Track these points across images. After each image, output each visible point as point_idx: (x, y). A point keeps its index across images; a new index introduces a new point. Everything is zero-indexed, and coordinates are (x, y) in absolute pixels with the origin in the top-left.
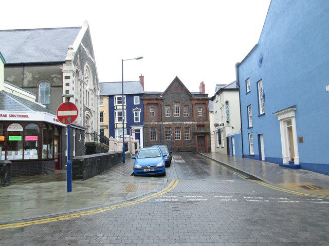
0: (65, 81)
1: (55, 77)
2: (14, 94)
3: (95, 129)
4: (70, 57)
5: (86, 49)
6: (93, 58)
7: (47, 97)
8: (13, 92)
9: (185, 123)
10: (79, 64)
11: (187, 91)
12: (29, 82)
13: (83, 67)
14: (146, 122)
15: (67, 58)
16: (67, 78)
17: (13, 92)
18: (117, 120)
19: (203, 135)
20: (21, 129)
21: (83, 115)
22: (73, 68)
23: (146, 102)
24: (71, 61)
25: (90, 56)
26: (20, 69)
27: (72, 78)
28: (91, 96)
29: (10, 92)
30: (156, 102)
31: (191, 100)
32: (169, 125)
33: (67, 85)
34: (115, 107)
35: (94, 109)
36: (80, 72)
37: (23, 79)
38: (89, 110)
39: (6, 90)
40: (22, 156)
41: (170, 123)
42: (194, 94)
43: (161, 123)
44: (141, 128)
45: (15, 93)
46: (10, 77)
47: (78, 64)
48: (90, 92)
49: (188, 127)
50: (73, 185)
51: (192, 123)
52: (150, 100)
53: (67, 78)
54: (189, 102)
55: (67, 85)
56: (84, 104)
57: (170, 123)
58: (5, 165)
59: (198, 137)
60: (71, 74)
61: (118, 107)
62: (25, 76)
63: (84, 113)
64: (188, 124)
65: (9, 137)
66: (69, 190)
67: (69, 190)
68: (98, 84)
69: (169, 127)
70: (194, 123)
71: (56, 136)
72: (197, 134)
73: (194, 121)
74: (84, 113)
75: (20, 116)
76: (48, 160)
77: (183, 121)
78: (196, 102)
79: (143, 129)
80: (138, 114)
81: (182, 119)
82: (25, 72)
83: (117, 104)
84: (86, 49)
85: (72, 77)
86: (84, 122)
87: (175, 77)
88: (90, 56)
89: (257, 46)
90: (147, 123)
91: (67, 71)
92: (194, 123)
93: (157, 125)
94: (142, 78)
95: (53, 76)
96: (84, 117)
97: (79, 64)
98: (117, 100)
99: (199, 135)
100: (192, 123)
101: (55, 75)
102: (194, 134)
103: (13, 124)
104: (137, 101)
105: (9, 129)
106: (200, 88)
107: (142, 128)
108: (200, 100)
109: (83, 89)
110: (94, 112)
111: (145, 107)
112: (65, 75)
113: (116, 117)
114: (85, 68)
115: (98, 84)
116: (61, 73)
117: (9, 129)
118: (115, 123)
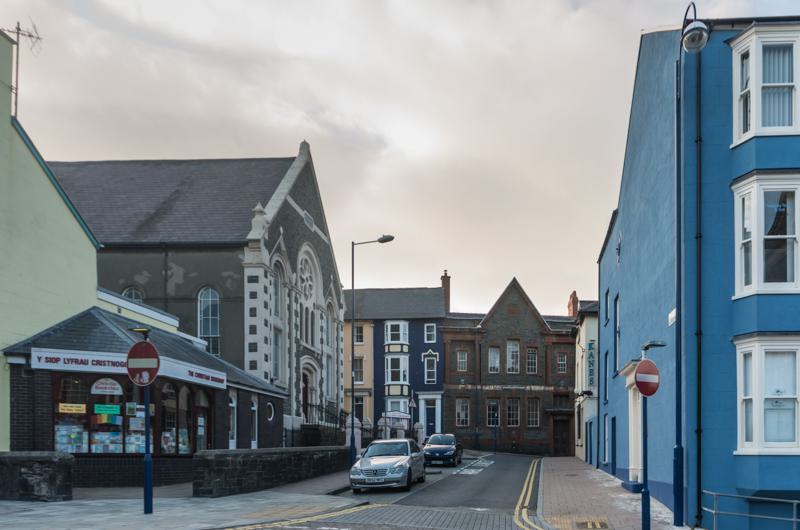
0: (249, 288)
1: (230, 277)
2: (122, 314)
3: (330, 396)
4: (257, 232)
5: (302, 213)
6: (326, 233)
7: (214, 321)
8: (119, 311)
9: (528, 388)
10: (283, 248)
11: (534, 312)
12: (178, 286)
13: (296, 254)
14: (450, 383)
15: (251, 236)
16: (254, 279)
17: (119, 311)
18: (390, 378)
19: (565, 418)
20: (118, 391)
21: (294, 365)
22: (265, 256)
23: (448, 338)
24: (258, 241)
25: (315, 228)
26: (158, 257)
27: (263, 281)
28: (318, 323)
29: (114, 310)
30: (469, 337)
31: (543, 335)
32: (495, 391)
33: (253, 295)
34: (387, 348)
35: (326, 349)
36: (287, 266)
37: (166, 281)
38: (311, 353)
39: (104, 306)
40: (121, 446)
41: (498, 387)
42: (551, 323)
43: (479, 387)
44: (437, 397)
45: (124, 313)
46: (141, 274)
47: (279, 250)
48: (317, 313)
49: (535, 397)
50: (155, 501)
51: (542, 388)
52: (474, 333)
53: (254, 279)
54: (539, 340)
55: (253, 295)
56: (296, 339)
57: (498, 387)
58: (56, 460)
59: (555, 421)
60: (259, 272)
61: (392, 349)
62: (169, 273)
63: (298, 363)
64: (535, 392)
65: (84, 412)
66: (148, 509)
67: (148, 509)
68: (338, 295)
69: (495, 395)
70: (547, 388)
71: (203, 408)
72: (554, 414)
73: (547, 384)
74: (298, 363)
75: (114, 364)
76: (90, 457)
77: (526, 385)
78: (555, 339)
79: (442, 400)
80: (430, 359)
81: (522, 378)
82: (171, 264)
83: (390, 342)
84: (302, 213)
85: (262, 279)
86: (298, 379)
87: (511, 279)
88: (315, 228)
89: (615, 213)
90: (453, 387)
91: (251, 265)
92: (547, 388)
93: (471, 390)
94: (446, 279)
95: (225, 274)
96: (298, 368)
97: (283, 248)
98: (389, 332)
99: (559, 418)
100: (542, 388)
101: (231, 273)
102: (545, 414)
103: (102, 380)
104: (430, 334)
105: (94, 391)
106: (569, 307)
107: (439, 397)
108: (563, 335)
109: (294, 306)
110: (329, 357)
111: (448, 347)
112: (248, 272)
113: (389, 371)
114: (301, 256)
115: (338, 295)
116: (240, 269)
117: (94, 391)
118: (387, 383)
